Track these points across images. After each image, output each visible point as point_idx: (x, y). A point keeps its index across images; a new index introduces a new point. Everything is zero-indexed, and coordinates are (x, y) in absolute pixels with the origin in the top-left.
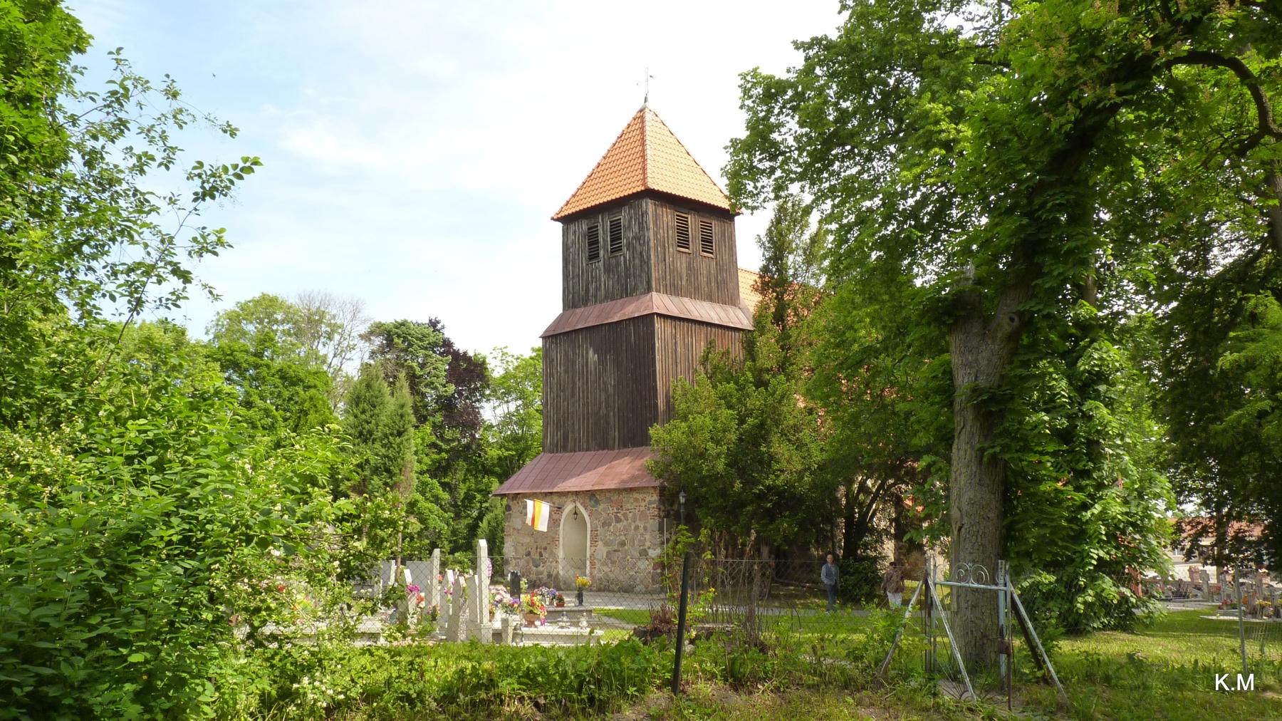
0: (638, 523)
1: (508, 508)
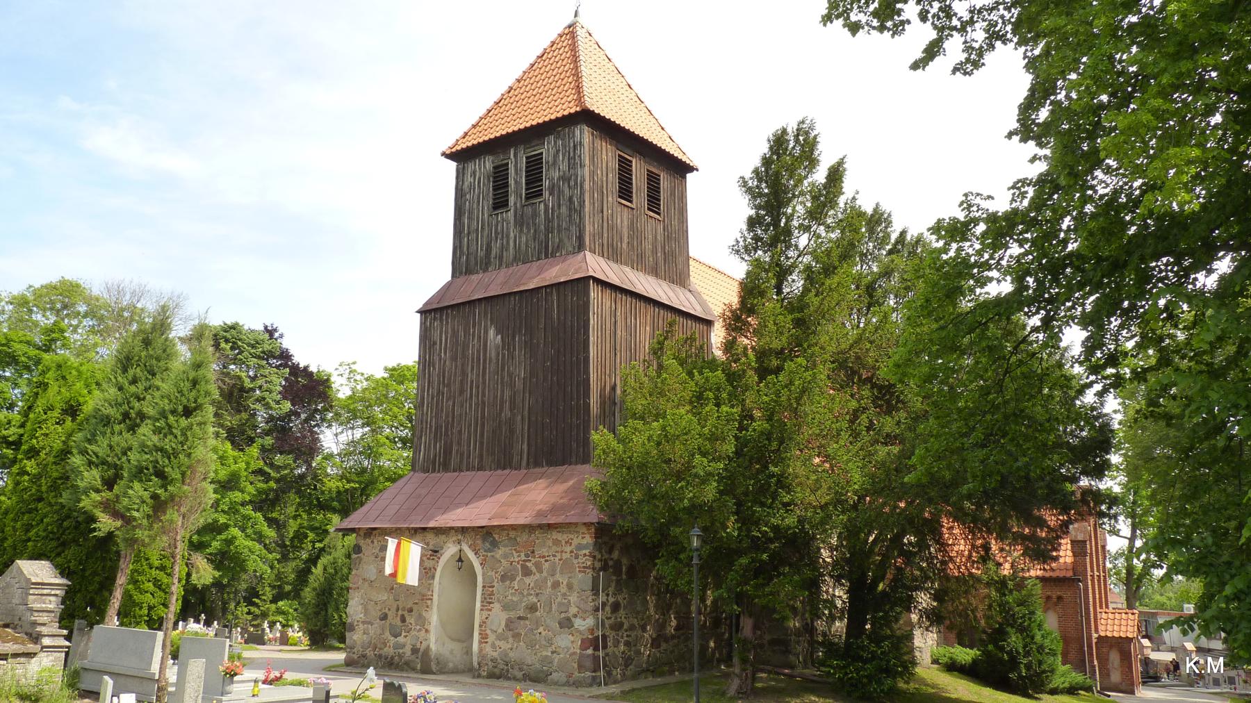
0: (558, 577)
1: (357, 549)
